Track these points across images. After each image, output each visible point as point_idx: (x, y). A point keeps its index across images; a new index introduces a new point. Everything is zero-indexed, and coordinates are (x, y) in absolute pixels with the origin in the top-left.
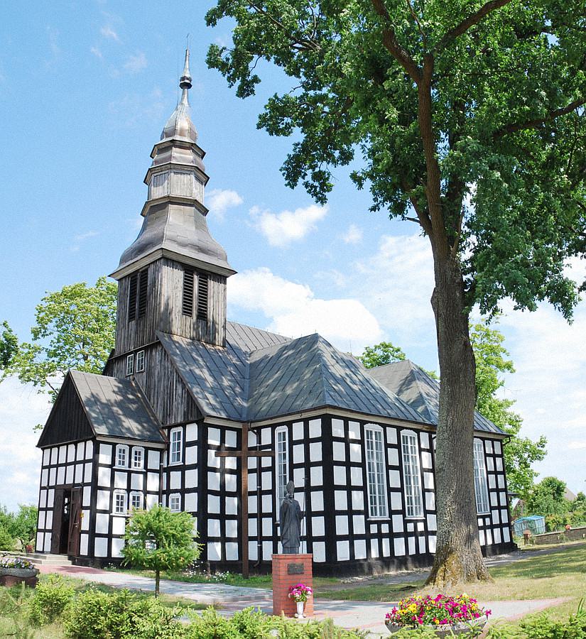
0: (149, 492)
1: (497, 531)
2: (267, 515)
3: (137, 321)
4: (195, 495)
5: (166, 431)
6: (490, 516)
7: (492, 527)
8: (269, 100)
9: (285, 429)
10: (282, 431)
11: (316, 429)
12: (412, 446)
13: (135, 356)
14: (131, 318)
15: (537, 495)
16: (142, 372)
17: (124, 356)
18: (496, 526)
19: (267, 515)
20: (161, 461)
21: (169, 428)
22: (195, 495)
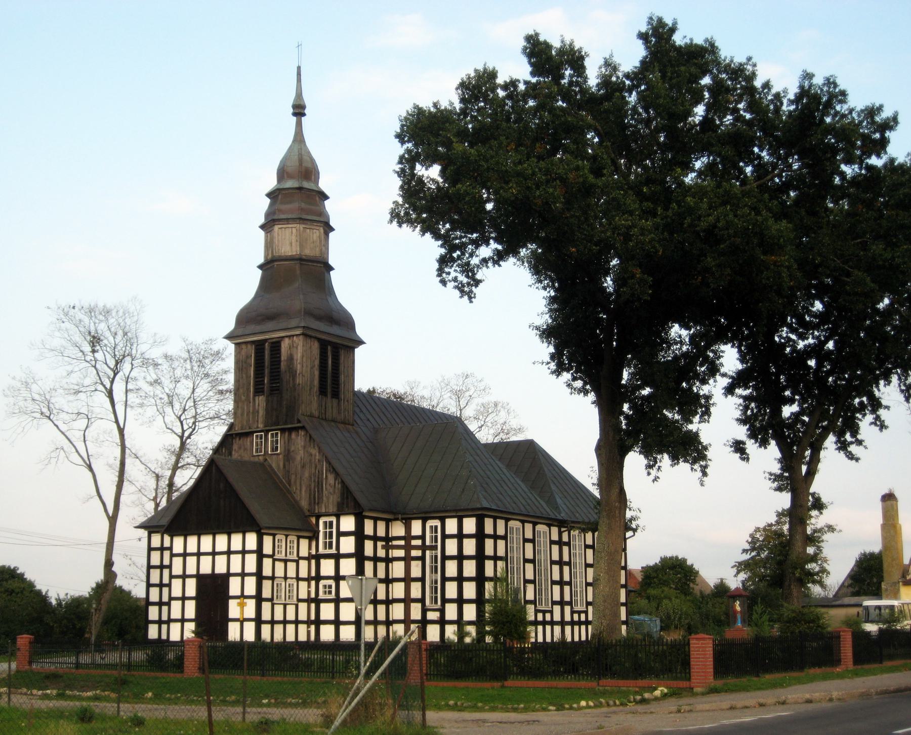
0: (344, 578)
1: (557, 629)
2: (416, 601)
3: (267, 397)
4: (474, 562)
5: (313, 520)
6: (551, 612)
7: (552, 623)
8: (394, 202)
9: (437, 523)
10: (434, 525)
11: (470, 525)
12: (543, 541)
13: (266, 436)
14: (258, 391)
15: (758, 213)
16: (278, 454)
17: (249, 434)
18: (557, 623)
19: (416, 601)
20: (310, 548)
21: (318, 517)
22: (474, 562)
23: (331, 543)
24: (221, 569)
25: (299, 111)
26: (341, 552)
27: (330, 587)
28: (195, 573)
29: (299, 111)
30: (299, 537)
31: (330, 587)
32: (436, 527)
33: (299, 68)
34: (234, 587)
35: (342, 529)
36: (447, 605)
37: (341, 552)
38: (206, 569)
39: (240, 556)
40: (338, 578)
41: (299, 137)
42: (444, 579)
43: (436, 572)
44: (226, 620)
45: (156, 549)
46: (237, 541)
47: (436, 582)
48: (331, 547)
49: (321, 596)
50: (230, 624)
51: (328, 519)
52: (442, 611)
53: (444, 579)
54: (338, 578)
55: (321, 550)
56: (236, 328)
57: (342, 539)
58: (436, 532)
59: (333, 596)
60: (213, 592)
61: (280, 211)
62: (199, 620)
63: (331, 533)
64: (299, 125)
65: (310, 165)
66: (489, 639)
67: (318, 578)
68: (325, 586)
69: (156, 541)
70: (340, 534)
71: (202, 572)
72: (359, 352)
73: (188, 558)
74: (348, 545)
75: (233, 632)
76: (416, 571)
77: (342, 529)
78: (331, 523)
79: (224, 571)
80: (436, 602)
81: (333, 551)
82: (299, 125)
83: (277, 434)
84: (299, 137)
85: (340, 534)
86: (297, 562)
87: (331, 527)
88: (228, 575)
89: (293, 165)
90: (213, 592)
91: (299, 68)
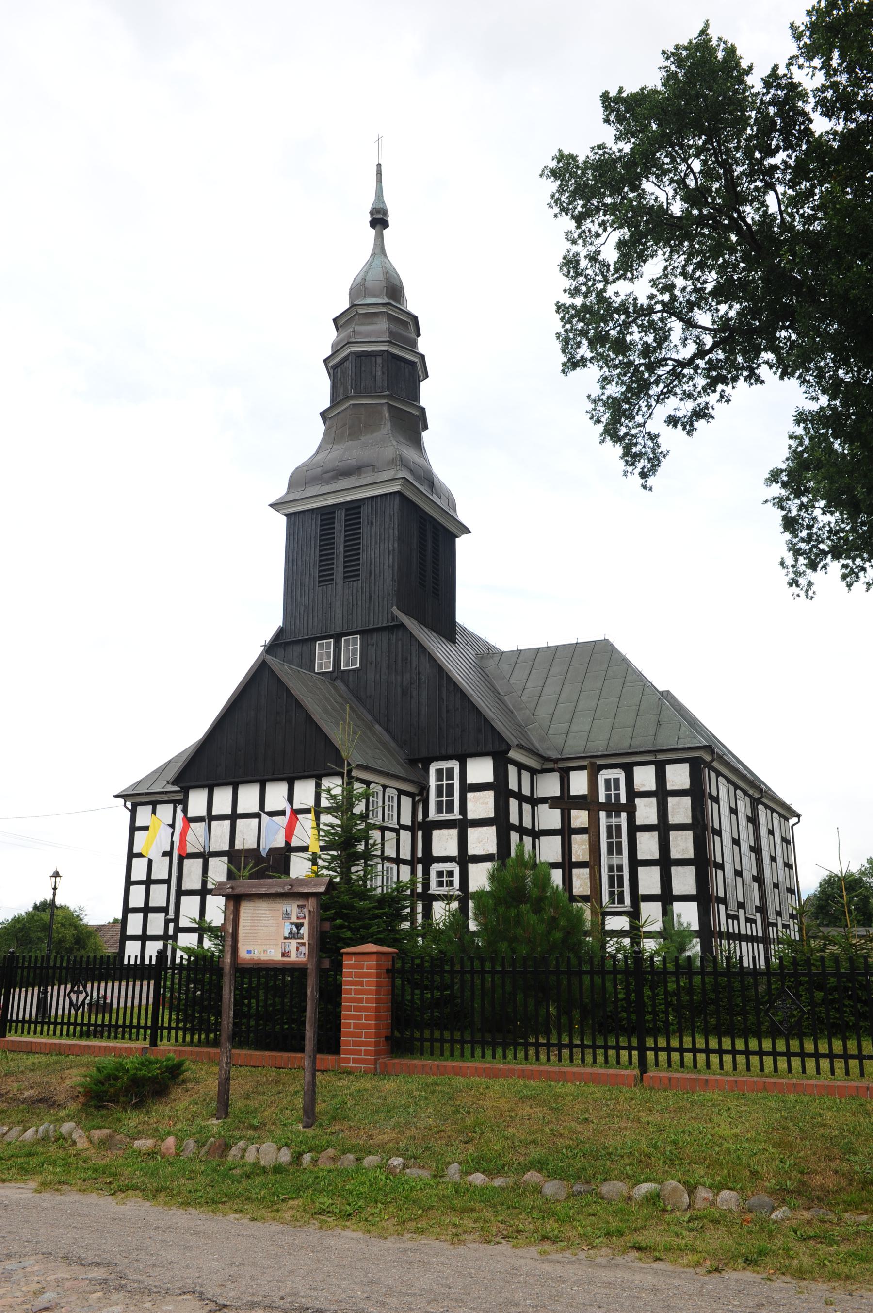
10: (612, 777)
14: (325, 577)
22: (689, 834)
23: (450, 804)
26: (470, 816)
27: (451, 874)
28: (226, 848)
30: (401, 792)
31: (451, 874)
32: (617, 781)
33: (379, 165)
35: (471, 779)
36: (130, 916)
37: (470, 816)
39: (152, 904)
40: (464, 859)
41: (380, 248)
42: (635, 863)
43: (620, 852)
45: (136, 910)
48: (450, 809)
49: (434, 889)
51: (444, 765)
52: (634, 914)
53: (635, 863)
54: (464, 859)
55: (433, 815)
56: (287, 493)
57: (184, 899)
61: (359, 333)
63: (450, 787)
64: (380, 238)
65: (398, 284)
67: (428, 859)
68: (440, 874)
70: (466, 788)
71: (238, 846)
72: (461, 543)
73: (228, 811)
74: (481, 805)
76: (580, 848)
77: (471, 779)
78: (450, 771)
79: (280, 843)
80: (621, 901)
81: (456, 815)
82: (380, 238)
83: (355, 640)
84: (380, 248)
85: (466, 788)
86: (397, 831)
87: (450, 777)
88: (289, 849)
89: (376, 278)
91: (379, 165)
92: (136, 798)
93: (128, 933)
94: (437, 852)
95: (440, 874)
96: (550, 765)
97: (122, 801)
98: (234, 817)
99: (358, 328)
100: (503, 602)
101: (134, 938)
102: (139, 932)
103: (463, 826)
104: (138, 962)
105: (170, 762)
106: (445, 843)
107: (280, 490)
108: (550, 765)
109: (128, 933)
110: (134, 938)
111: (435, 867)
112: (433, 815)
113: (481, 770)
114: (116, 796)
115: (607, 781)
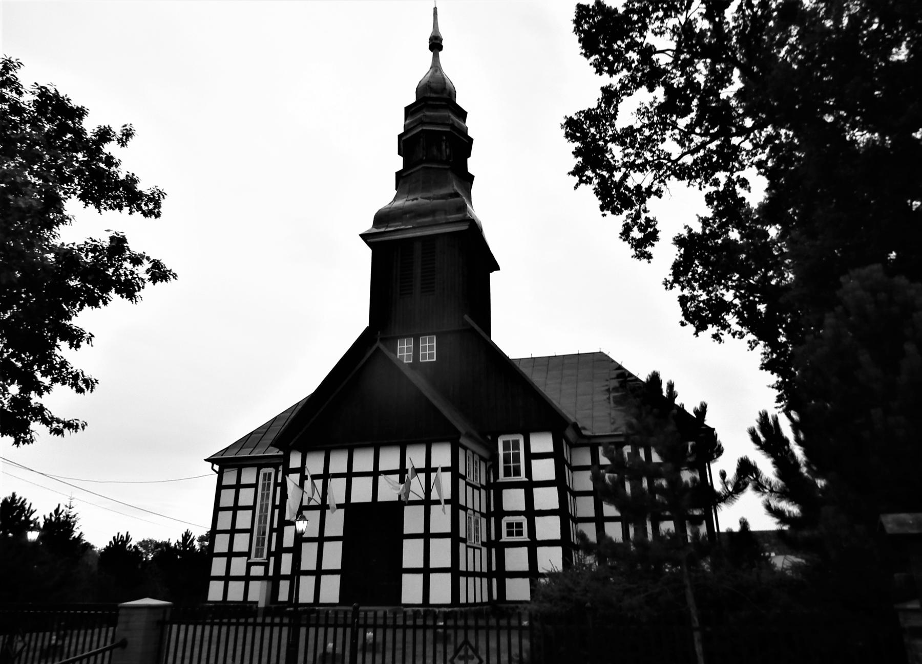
24: (389, 490)
25: (436, 44)
26: (535, 478)
27: (520, 525)
29: (436, 44)
32: (270, 474)
33: (435, 9)
34: (413, 520)
35: (534, 449)
37: (535, 478)
38: (362, 492)
41: (436, 65)
44: (397, 570)
46: (416, 457)
47: (264, 533)
48: (517, 473)
50: (405, 577)
51: (511, 438)
54: (531, 513)
55: (502, 478)
58: (269, 479)
59: (505, 538)
60: (374, 533)
62: (348, 572)
64: (436, 58)
66: (542, 581)
68: (510, 525)
69: (230, 478)
70: (531, 456)
74: (544, 470)
75: (411, 590)
77: (534, 449)
81: (523, 477)
82: (436, 58)
84: (436, 65)
90: (374, 533)
91: (435, 9)
92: (223, 462)
93: (303, 568)
94: (507, 506)
95: (510, 525)
96: (586, 441)
97: (210, 464)
98: (349, 475)
99: (428, 113)
100: (526, 323)
101: (308, 573)
102: (313, 567)
103: (529, 486)
104: (495, 597)
105: (252, 433)
106: (514, 499)
107: (367, 225)
108: (586, 441)
109: (303, 568)
110: (308, 573)
111: (506, 520)
112: (502, 478)
113: (542, 443)
114: (206, 460)
115: (265, 475)
